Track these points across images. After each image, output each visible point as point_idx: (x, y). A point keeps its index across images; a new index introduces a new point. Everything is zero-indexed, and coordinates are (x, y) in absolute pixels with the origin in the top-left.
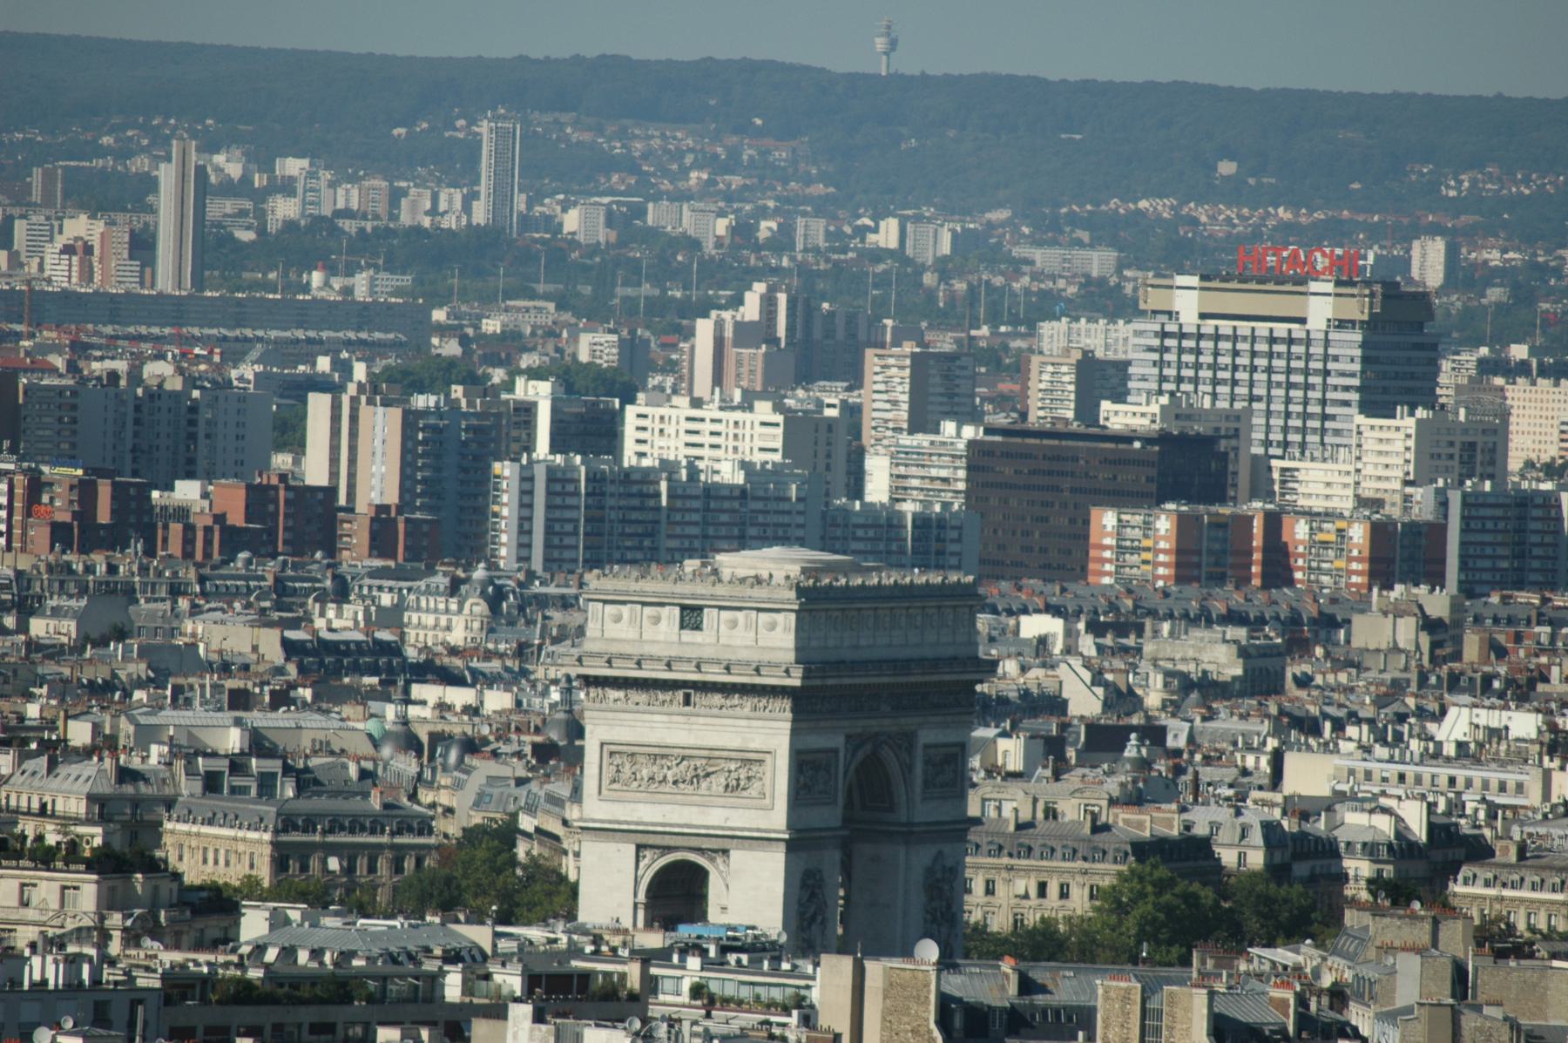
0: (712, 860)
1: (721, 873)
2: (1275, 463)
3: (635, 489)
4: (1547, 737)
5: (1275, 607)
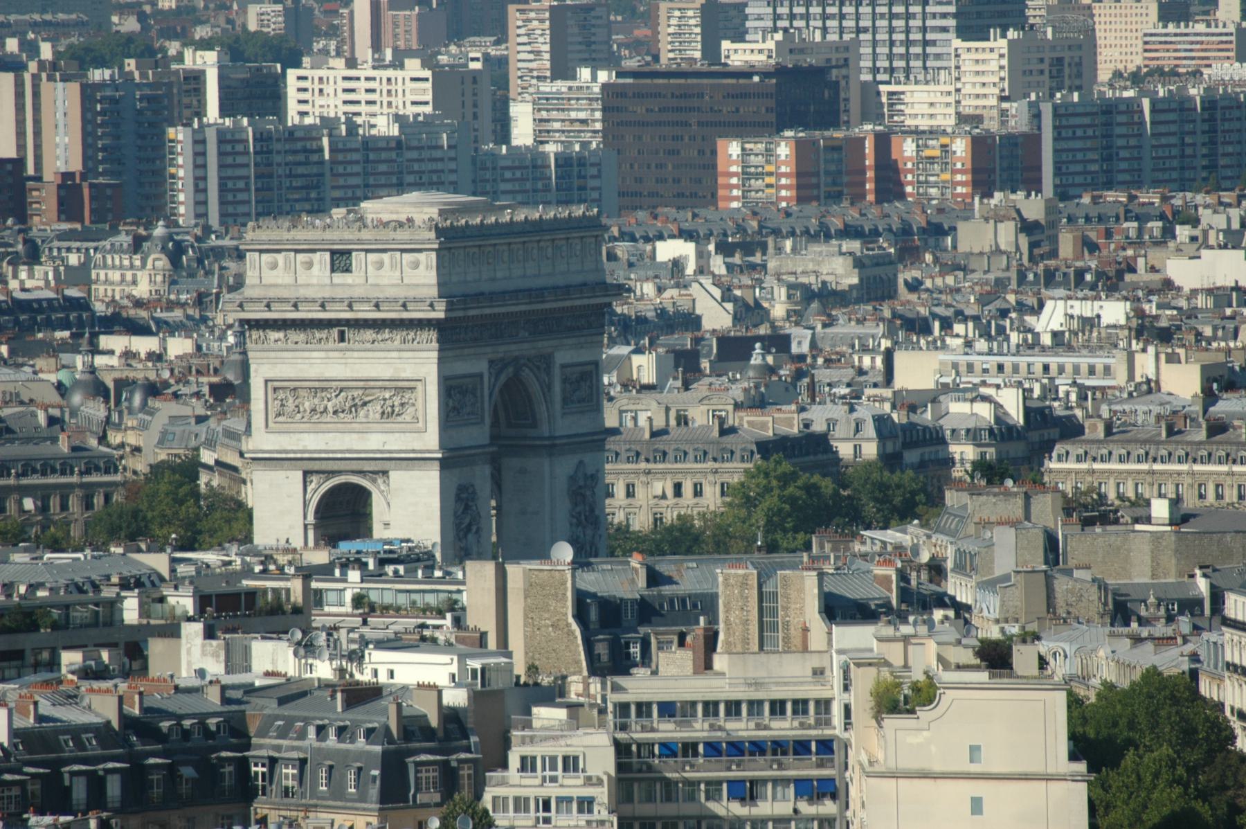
0: (374, 481)
1: (382, 492)
2: (882, 88)
3: (299, 145)
4: (1134, 323)
5: (887, 220)
